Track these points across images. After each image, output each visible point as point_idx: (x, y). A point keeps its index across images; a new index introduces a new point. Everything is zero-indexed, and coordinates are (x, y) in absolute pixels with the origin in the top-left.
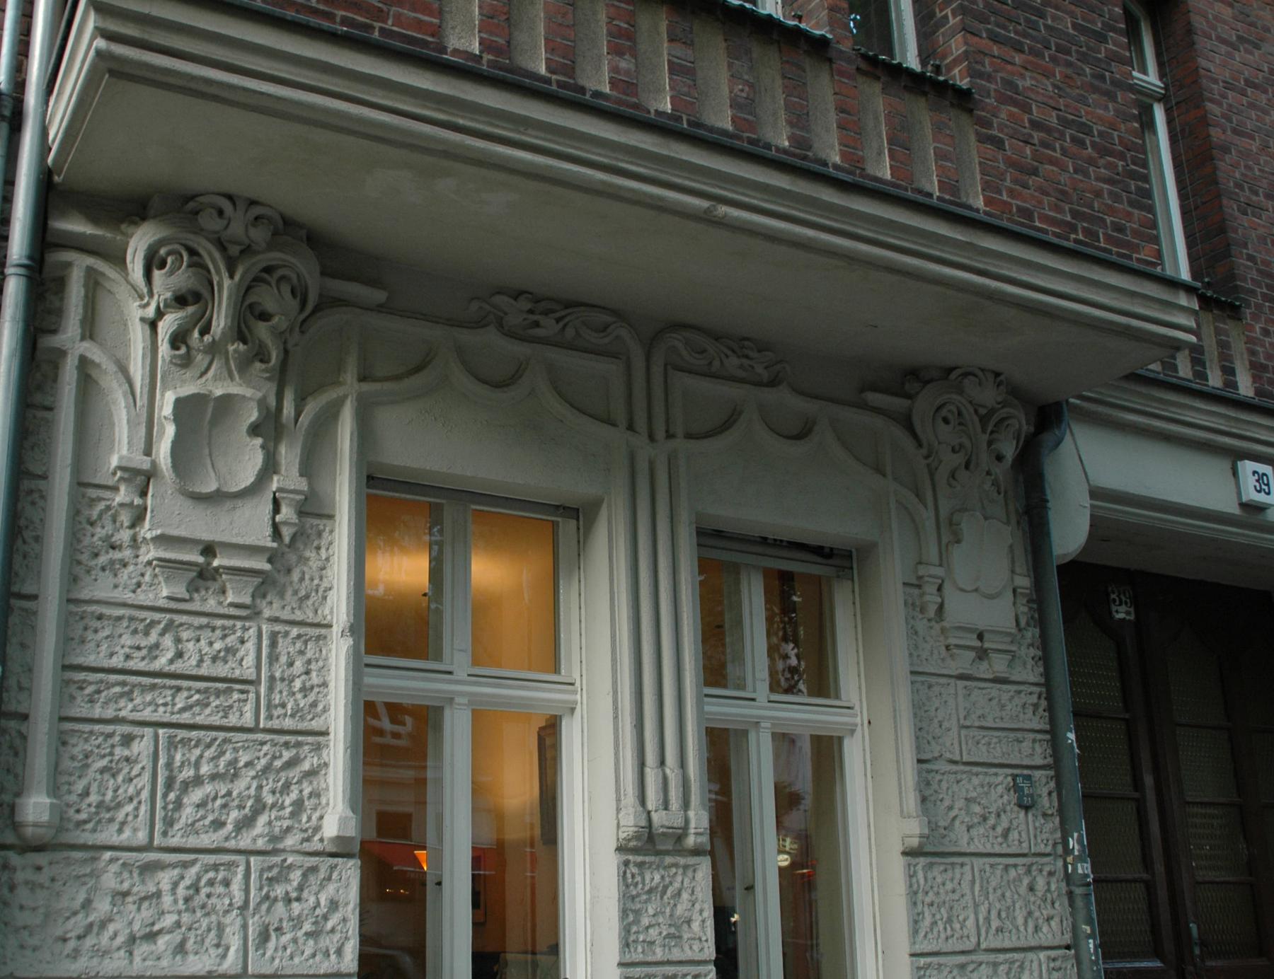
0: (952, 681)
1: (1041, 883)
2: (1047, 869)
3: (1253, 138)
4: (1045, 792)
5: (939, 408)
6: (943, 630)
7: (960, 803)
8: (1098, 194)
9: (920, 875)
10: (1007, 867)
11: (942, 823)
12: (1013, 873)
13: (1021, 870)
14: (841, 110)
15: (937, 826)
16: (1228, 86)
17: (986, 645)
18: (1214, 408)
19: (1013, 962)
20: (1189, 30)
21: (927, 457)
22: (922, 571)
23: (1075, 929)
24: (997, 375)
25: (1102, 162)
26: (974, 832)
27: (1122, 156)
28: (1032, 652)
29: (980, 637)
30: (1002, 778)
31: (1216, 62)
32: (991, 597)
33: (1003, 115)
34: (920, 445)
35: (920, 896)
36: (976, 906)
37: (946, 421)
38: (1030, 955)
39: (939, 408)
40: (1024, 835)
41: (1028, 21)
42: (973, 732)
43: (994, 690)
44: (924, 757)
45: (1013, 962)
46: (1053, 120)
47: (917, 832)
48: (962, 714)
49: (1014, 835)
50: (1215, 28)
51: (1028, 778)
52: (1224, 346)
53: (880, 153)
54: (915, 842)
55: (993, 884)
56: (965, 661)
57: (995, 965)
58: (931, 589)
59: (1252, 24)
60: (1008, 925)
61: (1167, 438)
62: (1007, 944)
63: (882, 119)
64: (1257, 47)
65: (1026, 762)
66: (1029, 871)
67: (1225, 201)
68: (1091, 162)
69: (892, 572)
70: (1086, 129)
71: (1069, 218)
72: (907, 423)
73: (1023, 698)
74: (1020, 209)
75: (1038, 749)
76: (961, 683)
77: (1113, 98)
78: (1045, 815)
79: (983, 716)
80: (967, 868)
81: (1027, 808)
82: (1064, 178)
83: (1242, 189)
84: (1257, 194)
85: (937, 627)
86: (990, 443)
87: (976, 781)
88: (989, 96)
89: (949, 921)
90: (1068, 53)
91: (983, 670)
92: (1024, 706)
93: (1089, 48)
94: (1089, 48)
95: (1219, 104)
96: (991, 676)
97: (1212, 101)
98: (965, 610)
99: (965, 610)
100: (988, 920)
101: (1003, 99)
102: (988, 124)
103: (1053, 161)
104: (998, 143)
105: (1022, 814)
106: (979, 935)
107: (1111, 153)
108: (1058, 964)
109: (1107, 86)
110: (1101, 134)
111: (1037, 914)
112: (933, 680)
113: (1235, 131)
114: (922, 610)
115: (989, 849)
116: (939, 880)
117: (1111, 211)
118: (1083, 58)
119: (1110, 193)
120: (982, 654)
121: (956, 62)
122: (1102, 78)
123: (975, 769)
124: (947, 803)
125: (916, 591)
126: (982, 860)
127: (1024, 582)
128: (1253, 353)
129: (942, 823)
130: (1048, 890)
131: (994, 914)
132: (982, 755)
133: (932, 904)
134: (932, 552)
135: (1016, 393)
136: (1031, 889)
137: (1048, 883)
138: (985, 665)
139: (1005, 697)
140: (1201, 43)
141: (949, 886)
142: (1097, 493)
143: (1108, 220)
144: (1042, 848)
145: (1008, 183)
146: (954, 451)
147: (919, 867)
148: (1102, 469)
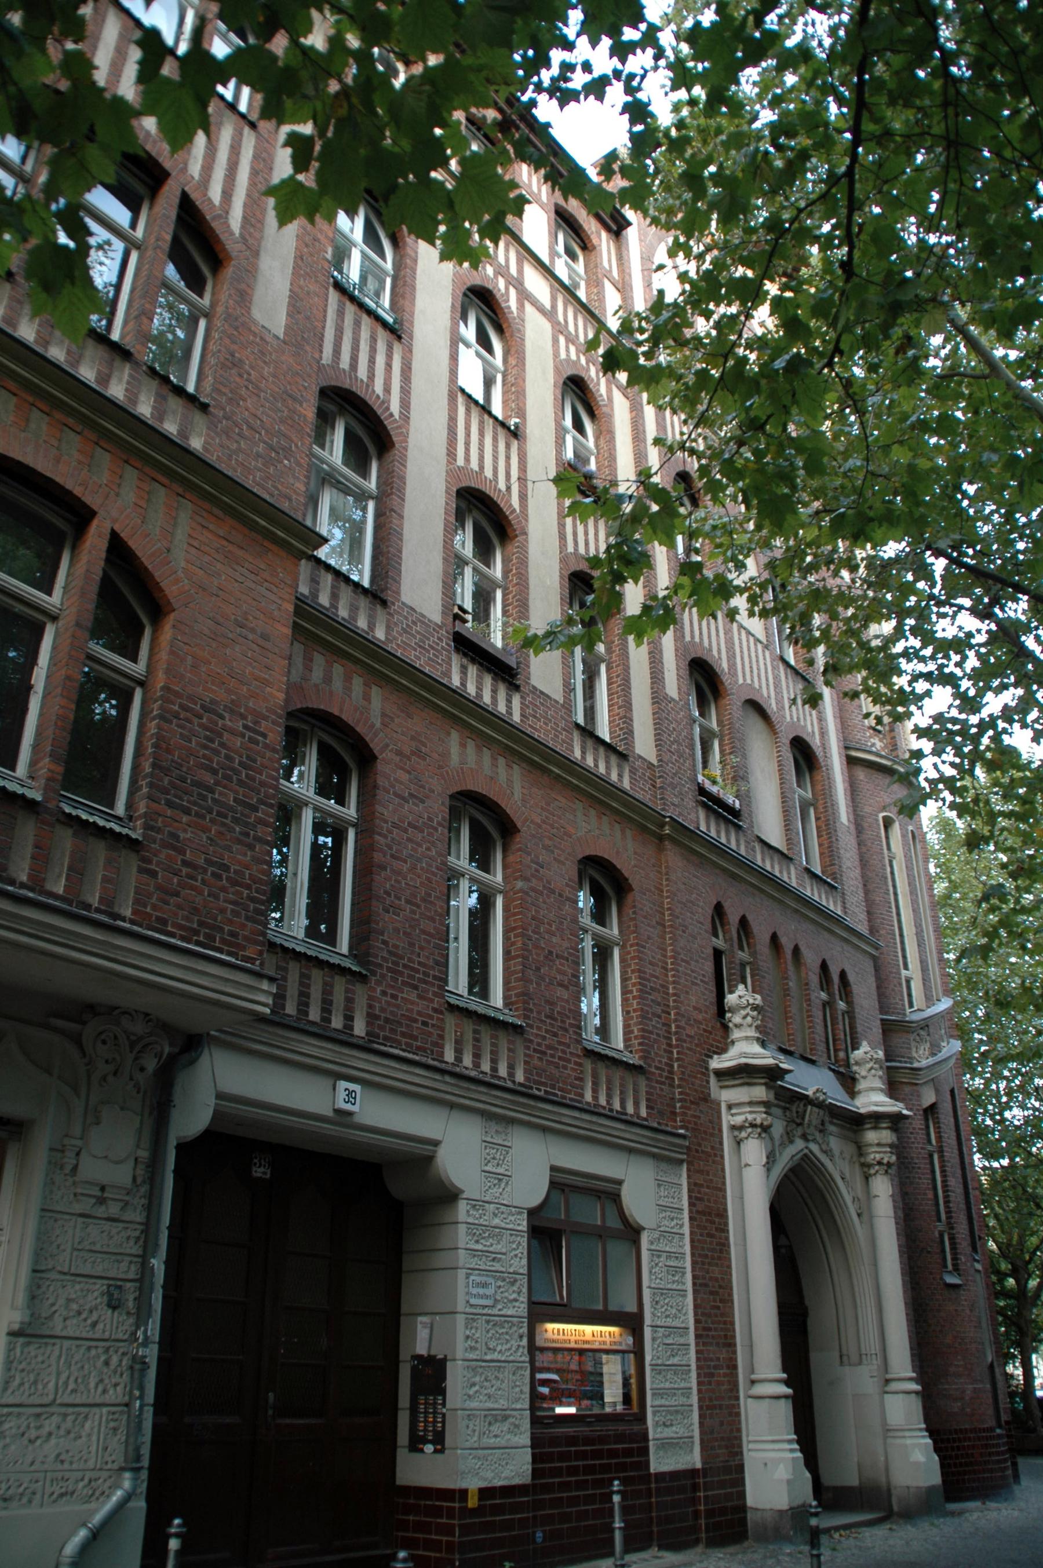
0: (74, 1218)
1: (115, 1360)
2: (121, 1350)
3: (405, 862)
4: (131, 1297)
5: (101, 1033)
6: (74, 1183)
7: (61, 1301)
8: (223, 911)
9: (18, 1350)
10: (89, 1348)
11: (44, 1315)
12: (93, 1352)
13: (100, 1350)
14: (37, 846)
15: (40, 1317)
16: (395, 825)
17: (106, 1195)
18: (324, 1044)
19: (79, 1414)
20: (375, 787)
21: (87, 1065)
22: (66, 1141)
23: (131, 1392)
24: (147, 1015)
25: (232, 890)
26: (68, 1322)
27: (248, 887)
28: (143, 1201)
29: (103, 1189)
30: (100, 1286)
31: (387, 809)
32: (117, 1163)
33: (162, 856)
34: (84, 1055)
35: (15, 1364)
36: (59, 1374)
37: (104, 1042)
38: (96, 1410)
39: (101, 1033)
40: (108, 1327)
41: (200, 794)
42: (81, 1254)
43: (107, 1226)
44: (39, 1268)
45: (79, 1414)
46: (201, 861)
47: (19, 1319)
48: (77, 1240)
49: (100, 1326)
50: (393, 787)
51: (120, 1287)
52: (349, 1000)
53: (60, 876)
54: (16, 1327)
55: (77, 1357)
56: (85, 1205)
57: (65, 1415)
58: (70, 1154)
59: (422, 787)
60: (82, 1387)
61: (286, 1062)
62: (78, 1401)
63: (68, 854)
64: (423, 802)
65: (122, 1276)
66: (107, 1350)
67: (374, 902)
68: (224, 889)
69: (42, 1141)
70: (226, 868)
71: (195, 926)
72: (77, 1040)
73: (129, 1233)
74: (158, 919)
75: (133, 1268)
76: (80, 1220)
77: (251, 847)
78: (128, 1313)
79: (94, 1243)
80: (58, 1347)
81: (114, 1308)
82: (198, 899)
83: (389, 895)
84: (399, 899)
85: (71, 1180)
86: (136, 1059)
87: (78, 1287)
88: (155, 842)
89: (35, 1382)
90: (226, 817)
91: (101, 1211)
92: (128, 1238)
93: (242, 814)
94: (242, 814)
95: (386, 837)
96: (105, 1216)
97: (380, 834)
98: (92, 1169)
99: (92, 1169)
100: (66, 1384)
101: (165, 845)
102: (150, 862)
103: (193, 888)
104: (153, 874)
105: (110, 1312)
106: (56, 1394)
107: (241, 885)
108: (116, 1416)
109: (250, 840)
110: (235, 871)
111: (107, 1381)
112: (58, 1216)
113: (392, 856)
114: (62, 1168)
115: (77, 1334)
116: (33, 1354)
117: (230, 922)
118: (236, 820)
119: (233, 911)
120: (101, 1201)
121: (140, 817)
122: (248, 835)
123: (78, 1279)
124: (50, 1301)
125: (59, 1155)
126: (70, 1342)
127: (144, 1154)
128: (370, 1006)
129: (44, 1315)
130: (120, 1365)
131: (72, 1379)
132: (87, 1270)
133: (23, 1370)
134: (77, 1130)
135: (166, 1028)
136: (107, 1363)
137: (121, 1361)
138: (103, 1208)
139: (114, 1231)
140: (381, 794)
141: (40, 1359)
142: (220, 1096)
143: (226, 928)
144: (120, 1336)
145: (154, 900)
146: (107, 1062)
147: (18, 1345)
148: (230, 1080)
